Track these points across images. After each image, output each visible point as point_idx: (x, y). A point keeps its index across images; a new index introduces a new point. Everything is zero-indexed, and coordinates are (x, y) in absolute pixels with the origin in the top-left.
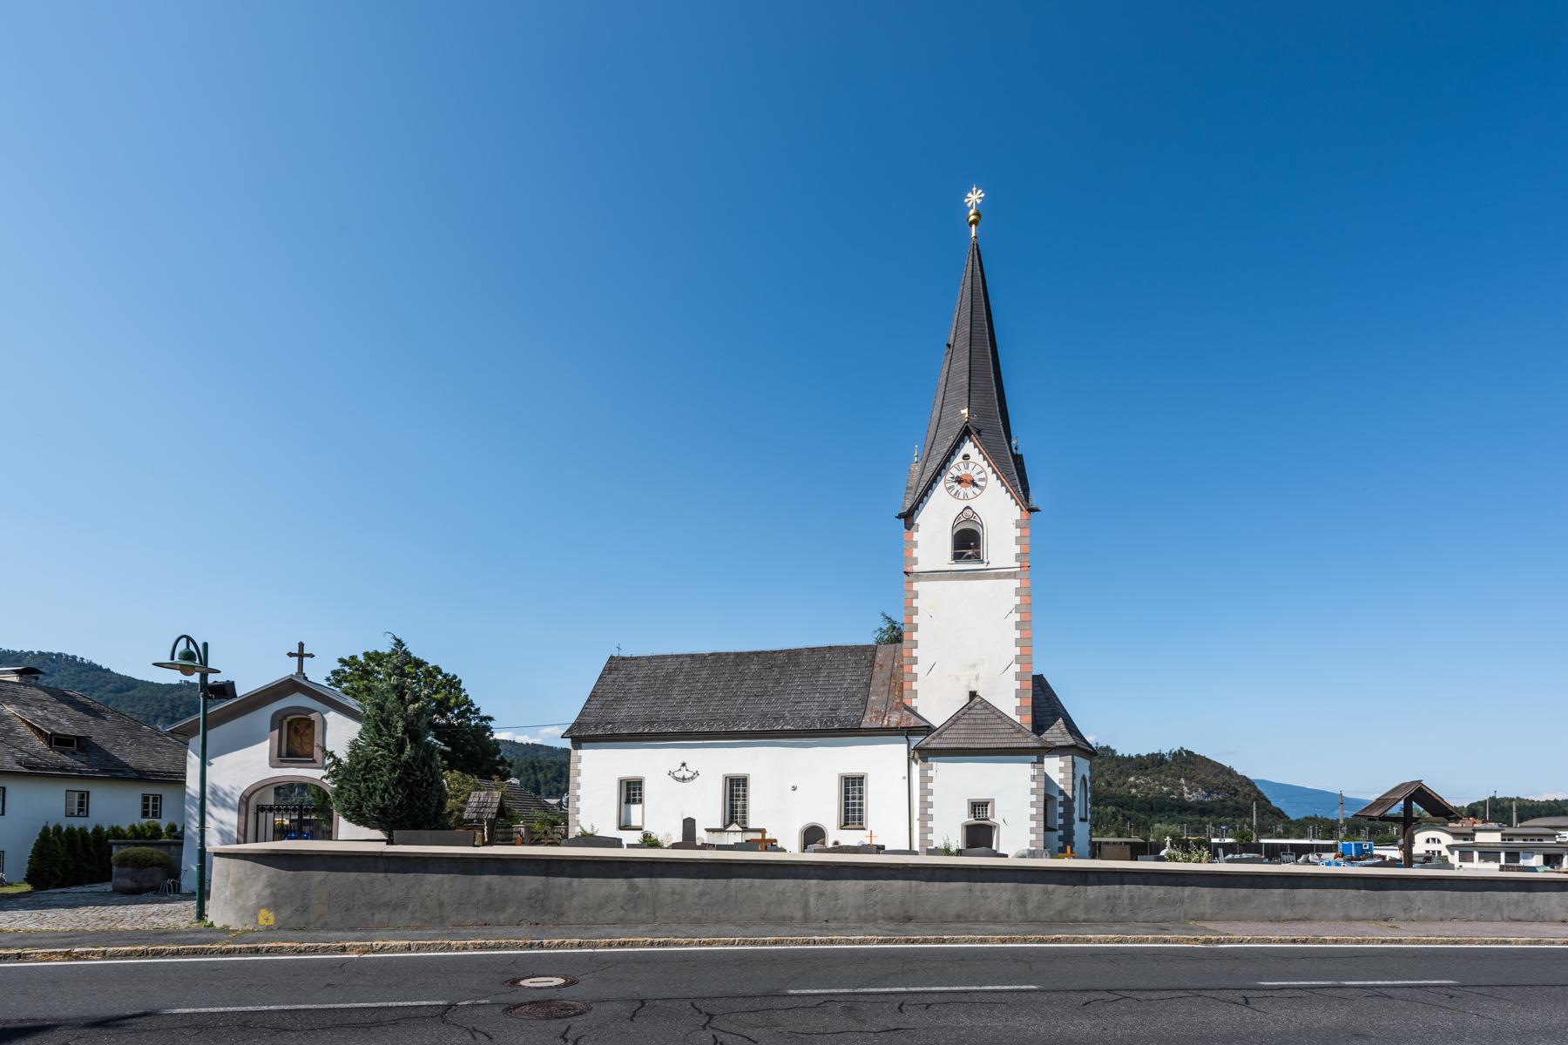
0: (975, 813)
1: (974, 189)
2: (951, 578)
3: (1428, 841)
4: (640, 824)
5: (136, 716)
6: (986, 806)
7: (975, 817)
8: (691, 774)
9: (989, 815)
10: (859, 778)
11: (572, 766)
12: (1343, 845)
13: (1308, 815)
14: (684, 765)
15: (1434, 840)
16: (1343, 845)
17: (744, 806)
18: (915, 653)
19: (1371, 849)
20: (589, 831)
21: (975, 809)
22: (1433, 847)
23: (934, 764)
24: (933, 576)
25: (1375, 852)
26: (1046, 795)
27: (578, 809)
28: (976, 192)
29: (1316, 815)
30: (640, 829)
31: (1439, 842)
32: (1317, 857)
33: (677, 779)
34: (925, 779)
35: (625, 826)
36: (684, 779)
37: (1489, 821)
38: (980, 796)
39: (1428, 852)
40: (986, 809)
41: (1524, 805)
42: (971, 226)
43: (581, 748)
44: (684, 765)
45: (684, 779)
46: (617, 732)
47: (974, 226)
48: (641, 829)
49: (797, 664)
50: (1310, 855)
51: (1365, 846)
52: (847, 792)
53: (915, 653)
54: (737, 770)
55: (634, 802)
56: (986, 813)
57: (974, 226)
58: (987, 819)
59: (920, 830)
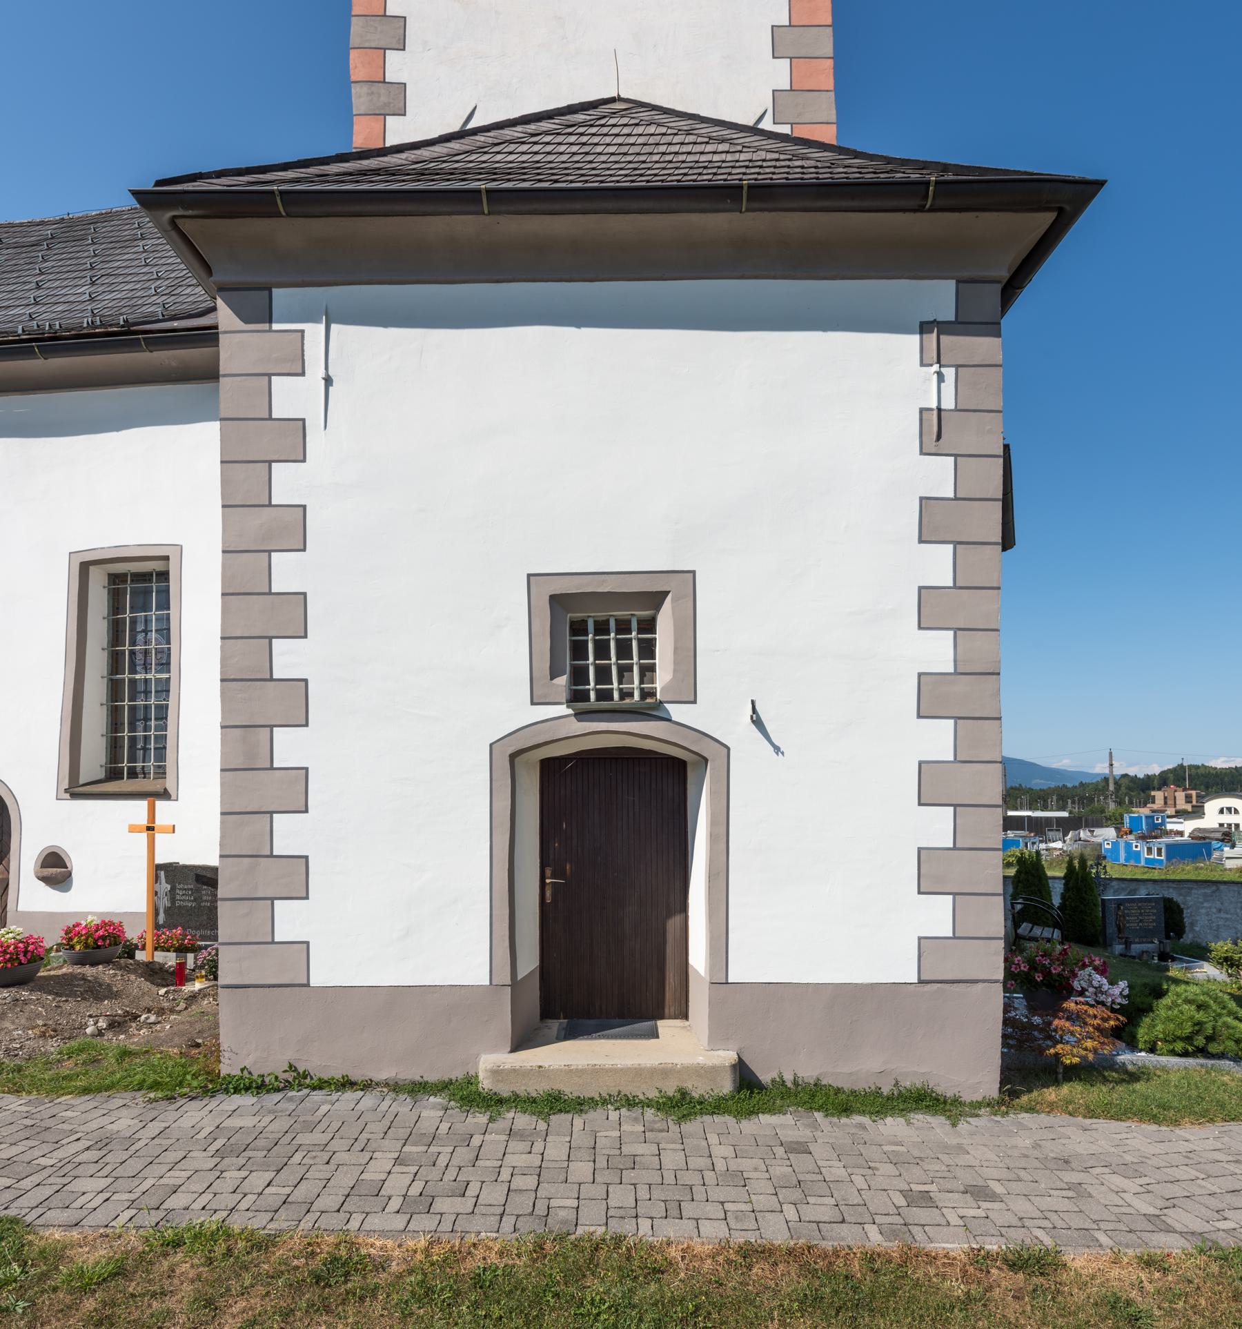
0: (579, 676)
3: (1221, 811)
6: (648, 626)
7: (577, 697)
9: (663, 678)
12: (1130, 817)
13: (1014, 786)
15: (1229, 809)
16: (1130, 817)
17: (162, 739)
18: (397, 66)
19: (1163, 823)
21: (579, 651)
22: (1228, 819)
23: (314, 332)
25: (1169, 827)
29: (1020, 785)
31: (1236, 812)
32: (1089, 834)
37: (1189, 789)
39: (1222, 825)
40: (648, 649)
41: (1209, 772)
49: (1087, 1107)
50: (1082, 832)
51: (1157, 819)
53: (397, 66)
56: (648, 671)
58: (650, 709)
59: (227, 790)
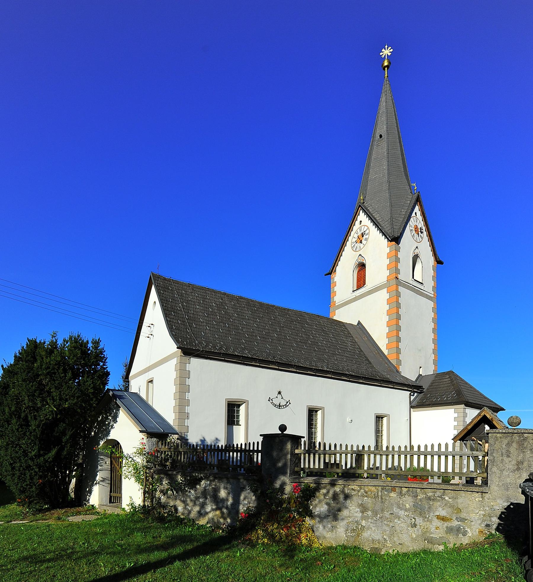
14: (279, 393)
44: (279, 393)
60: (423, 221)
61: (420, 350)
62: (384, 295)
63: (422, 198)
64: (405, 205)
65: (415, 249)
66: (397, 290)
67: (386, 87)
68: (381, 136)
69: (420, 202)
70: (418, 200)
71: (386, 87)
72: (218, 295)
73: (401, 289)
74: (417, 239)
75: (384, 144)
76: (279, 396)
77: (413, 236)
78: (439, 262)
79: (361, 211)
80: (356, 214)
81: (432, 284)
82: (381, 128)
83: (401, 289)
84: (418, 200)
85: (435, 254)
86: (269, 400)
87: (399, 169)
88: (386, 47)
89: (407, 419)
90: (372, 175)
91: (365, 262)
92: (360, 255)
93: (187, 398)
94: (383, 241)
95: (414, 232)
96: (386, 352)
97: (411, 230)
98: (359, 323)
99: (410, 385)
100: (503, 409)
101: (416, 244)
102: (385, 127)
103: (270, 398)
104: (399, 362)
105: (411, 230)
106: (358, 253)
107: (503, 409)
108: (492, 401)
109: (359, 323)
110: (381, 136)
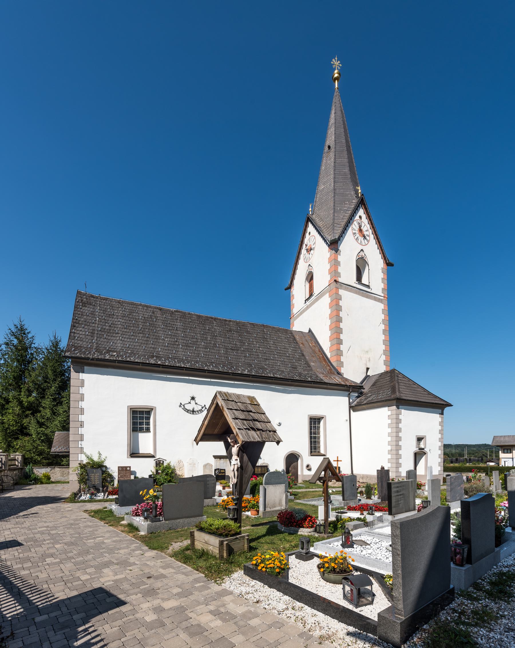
1: (341, 65)
2: (356, 293)
4: (152, 452)
5: (80, 315)
8: (200, 408)
10: (318, 419)
11: (72, 389)
14: (193, 398)
20: (96, 459)
24: (348, 288)
26: (68, 430)
27: (82, 435)
28: (339, 66)
30: (324, 455)
33: (188, 411)
34: (398, 421)
35: (134, 454)
36: (193, 412)
38: (421, 434)
42: (335, 82)
43: (83, 372)
44: (193, 398)
45: (193, 412)
46: (128, 359)
47: (336, 81)
48: (153, 457)
52: (311, 429)
54: (140, 402)
55: (141, 430)
57: (336, 81)
60: (369, 223)
61: (367, 352)
62: (326, 300)
63: (367, 201)
64: (349, 209)
65: (360, 252)
66: (337, 293)
67: (336, 100)
68: (329, 147)
69: (364, 205)
70: (362, 203)
71: (336, 100)
72: (150, 309)
73: (341, 292)
74: (361, 242)
75: (332, 155)
76: (193, 402)
77: (357, 239)
78: (389, 264)
79: (310, 223)
80: (306, 226)
81: (382, 286)
82: (330, 140)
83: (341, 292)
84: (362, 203)
85: (384, 257)
86: (180, 406)
87: (346, 177)
88: (341, 65)
89: (346, 419)
90: (321, 187)
91: (312, 271)
92: (309, 265)
93: (80, 407)
94: (325, 248)
95: (358, 235)
96: (329, 355)
97: (354, 234)
98: (310, 331)
99: (347, 385)
100: (450, 405)
101: (361, 247)
102: (333, 137)
103: (181, 404)
104: (342, 364)
105: (354, 234)
106: (308, 264)
107: (450, 405)
108: (429, 393)
109: (310, 331)
110: (329, 147)
